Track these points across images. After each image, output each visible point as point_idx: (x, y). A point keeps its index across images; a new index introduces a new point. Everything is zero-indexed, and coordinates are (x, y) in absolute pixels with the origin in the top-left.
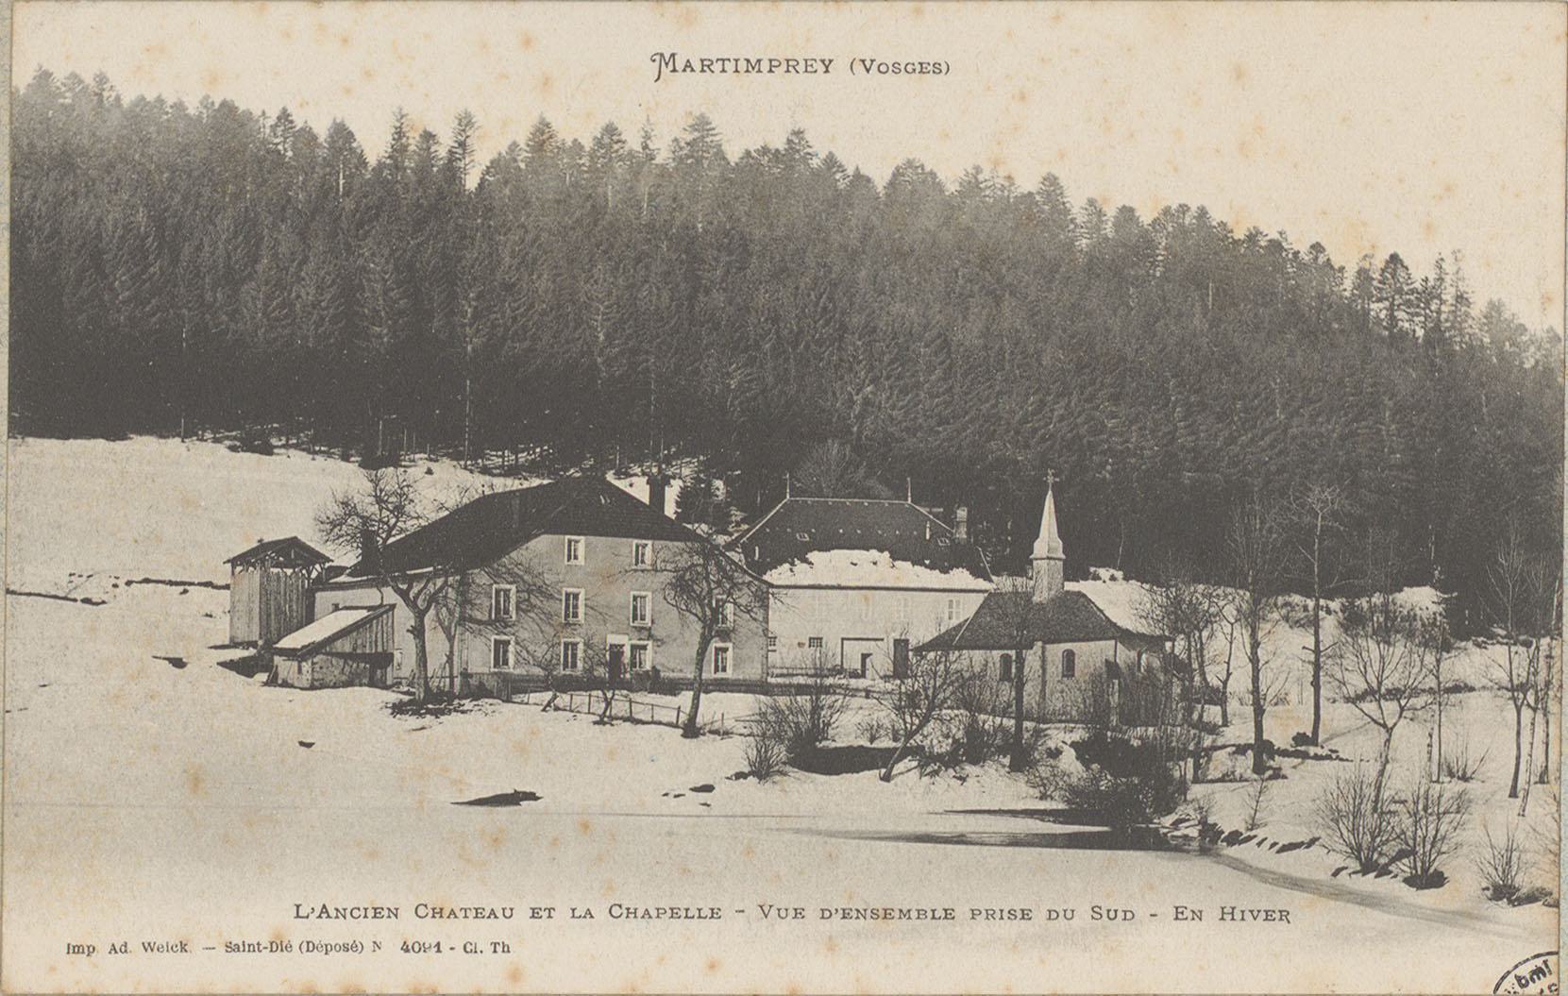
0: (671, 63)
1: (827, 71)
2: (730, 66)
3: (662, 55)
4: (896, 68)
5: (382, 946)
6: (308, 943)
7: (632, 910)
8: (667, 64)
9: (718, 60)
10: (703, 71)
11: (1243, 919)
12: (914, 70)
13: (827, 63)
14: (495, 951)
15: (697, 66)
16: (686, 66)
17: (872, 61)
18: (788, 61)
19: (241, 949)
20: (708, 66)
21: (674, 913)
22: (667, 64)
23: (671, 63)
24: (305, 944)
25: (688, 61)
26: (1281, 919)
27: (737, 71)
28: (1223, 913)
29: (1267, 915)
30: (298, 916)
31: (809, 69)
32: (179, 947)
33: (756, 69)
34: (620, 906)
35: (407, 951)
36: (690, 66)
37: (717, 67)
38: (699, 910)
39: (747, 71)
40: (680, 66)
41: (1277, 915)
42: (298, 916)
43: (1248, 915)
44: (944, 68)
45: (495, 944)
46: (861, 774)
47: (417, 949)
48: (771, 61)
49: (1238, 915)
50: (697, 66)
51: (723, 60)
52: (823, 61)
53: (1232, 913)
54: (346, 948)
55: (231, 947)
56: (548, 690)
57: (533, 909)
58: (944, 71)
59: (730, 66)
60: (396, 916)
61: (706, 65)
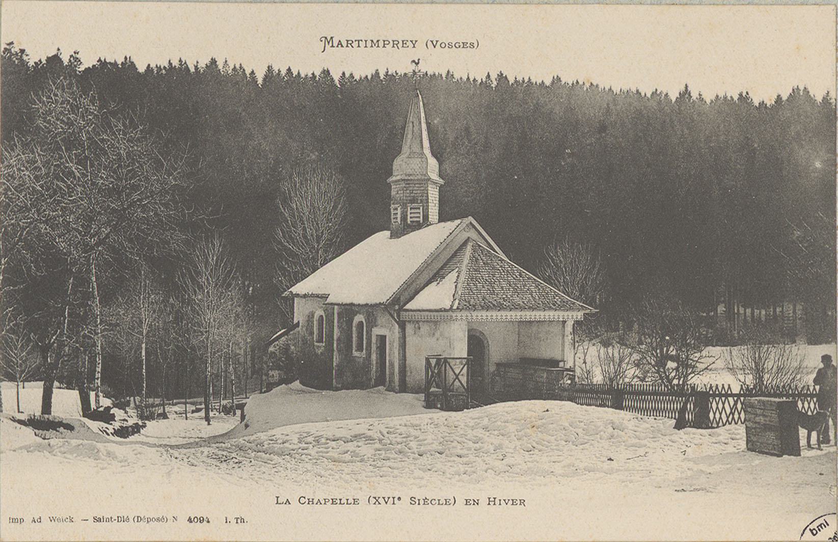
0: (331, 42)
1: (414, 47)
2: (362, 44)
3: (326, 38)
4: (450, 46)
5: (178, 519)
6: (138, 517)
7: (311, 500)
8: (329, 43)
9: (356, 41)
10: (347, 46)
11: (500, 504)
12: (460, 46)
13: (414, 42)
14: (237, 523)
15: (344, 44)
16: (338, 44)
17: (437, 41)
18: (393, 41)
19: (102, 520)
20: (397, 44)
21: (333, 502)
22: (329, 43)
23: (331, 42)
24: (136, 518)
25: (340, 41)
26: (520, 504)
27: (366, 47)
28: (489, 501)
29: (333, 502)
30: (277, 503)
31: (405, 45)
32: (69, 520)
33: (377, 45)
34: (305, 498)
35: (191, 522)
36: (341, 44)
37: (355, 44)
38: (347, 500)
39: (372, 46)
40: (335, 44)
41: (518, 502)
42: (277, 503)
43: (502, 502)
44: (476, 45)
45: (237, 519)
46: (96, 422)
47: (196, 521)
48: (384, 41)
49: (497, 502)
50: (344, 44)
51: (359, 41)
52: (412, 41)
53: (494, 501)
54: (158, 520)
55: (97, 520)
56: (42, 381)
57: (467, 500)
58: (476, 47)
59: (362, 44)
60: (478, 504)
61: (349, 43)
